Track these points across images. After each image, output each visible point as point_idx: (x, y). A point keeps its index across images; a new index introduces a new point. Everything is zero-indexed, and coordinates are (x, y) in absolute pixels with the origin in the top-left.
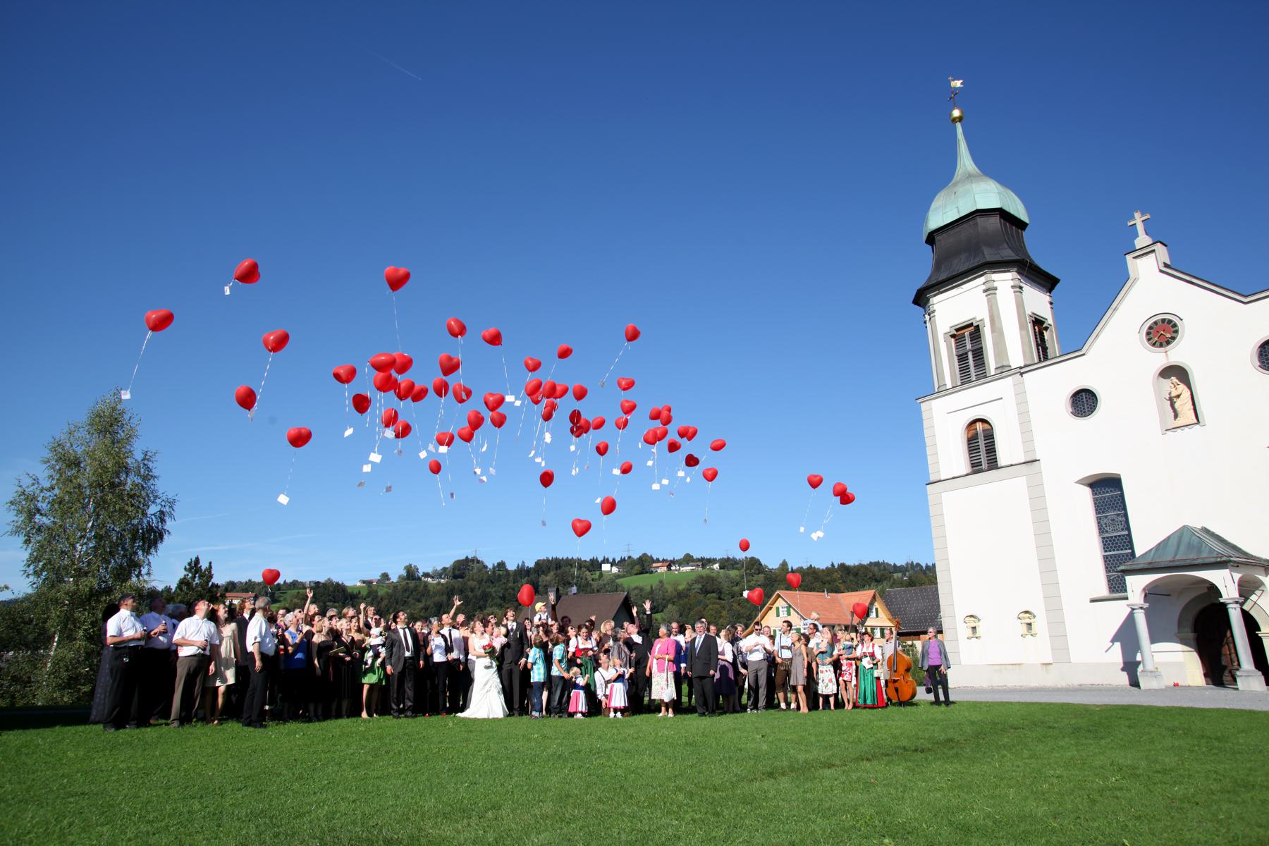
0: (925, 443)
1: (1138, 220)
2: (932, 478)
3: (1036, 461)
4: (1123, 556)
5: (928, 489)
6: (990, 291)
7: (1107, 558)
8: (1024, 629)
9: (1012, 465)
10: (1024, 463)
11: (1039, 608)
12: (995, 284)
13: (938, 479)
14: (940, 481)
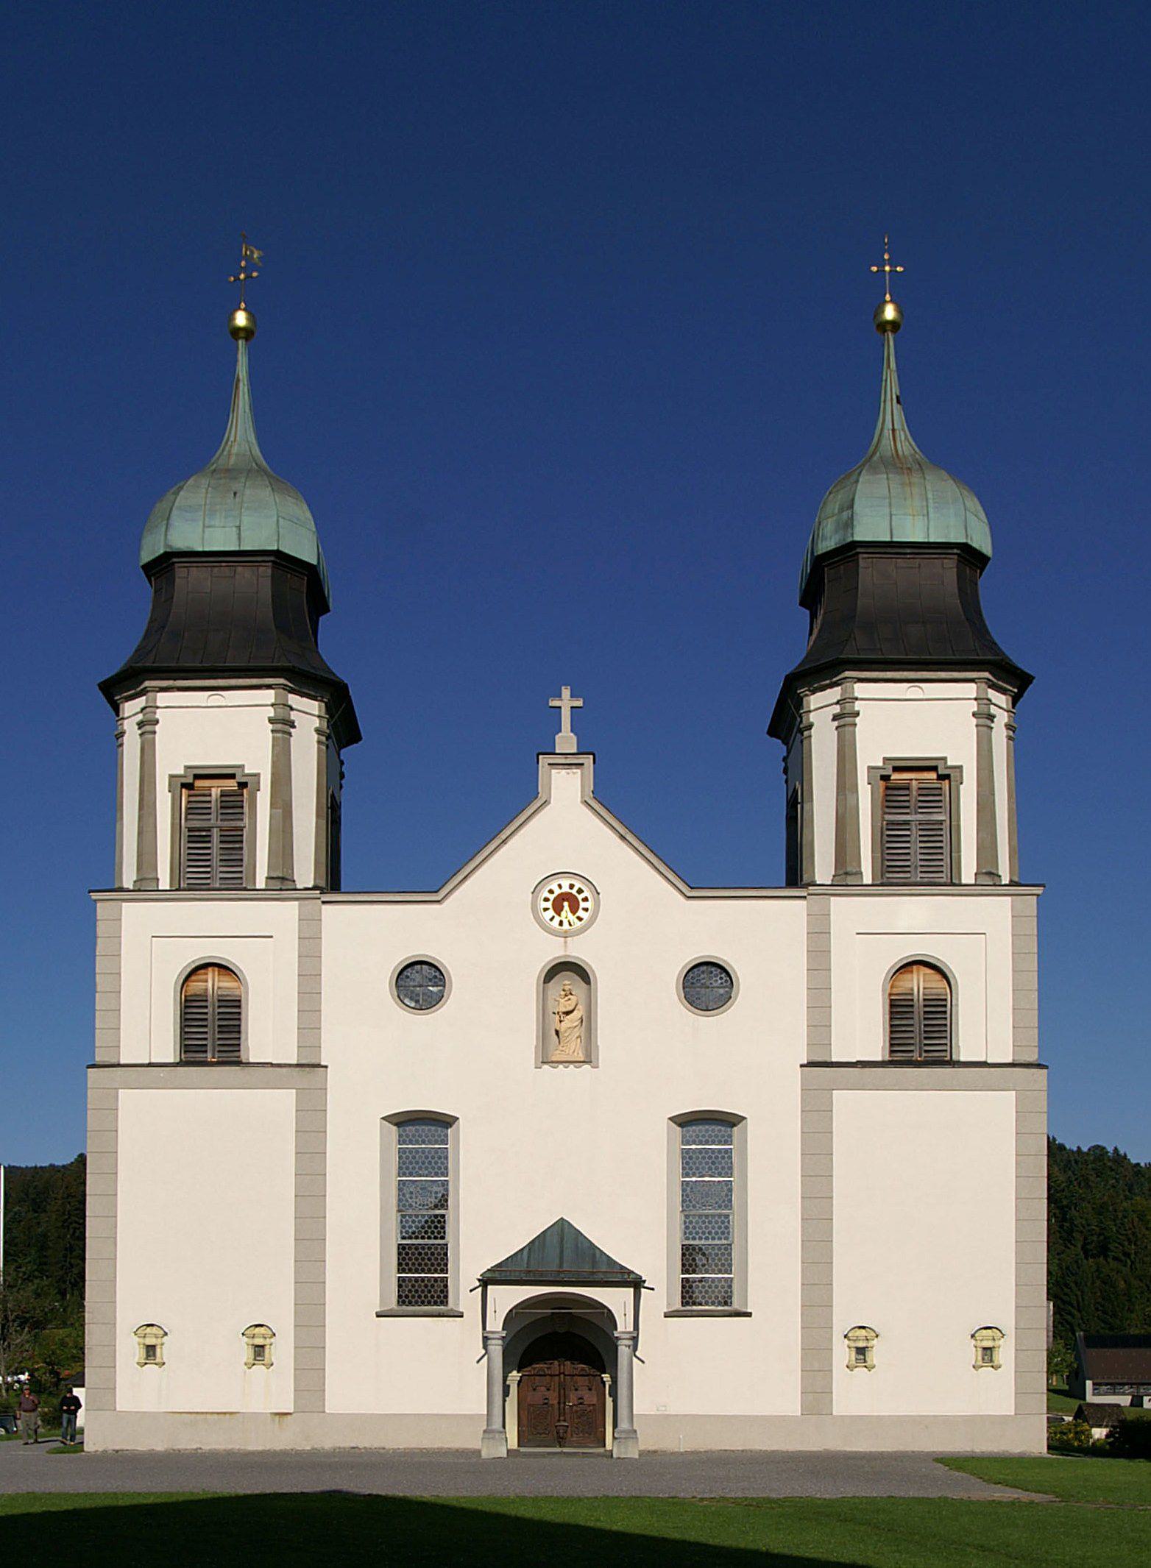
0: (95, 985)
1: (566, 702)
2: (99, 1059)
3: (319, 1066)
4: (423, 1249)
5: (89, 1075)
6: (283, 725)
7: (404, 1249)
8: (248, 1354)
9: (272, 1065)
10: (298, 1065)
11: (283, 1321)
12: (294, 716)
13: (114, 1061)
14: (119, 1065)
